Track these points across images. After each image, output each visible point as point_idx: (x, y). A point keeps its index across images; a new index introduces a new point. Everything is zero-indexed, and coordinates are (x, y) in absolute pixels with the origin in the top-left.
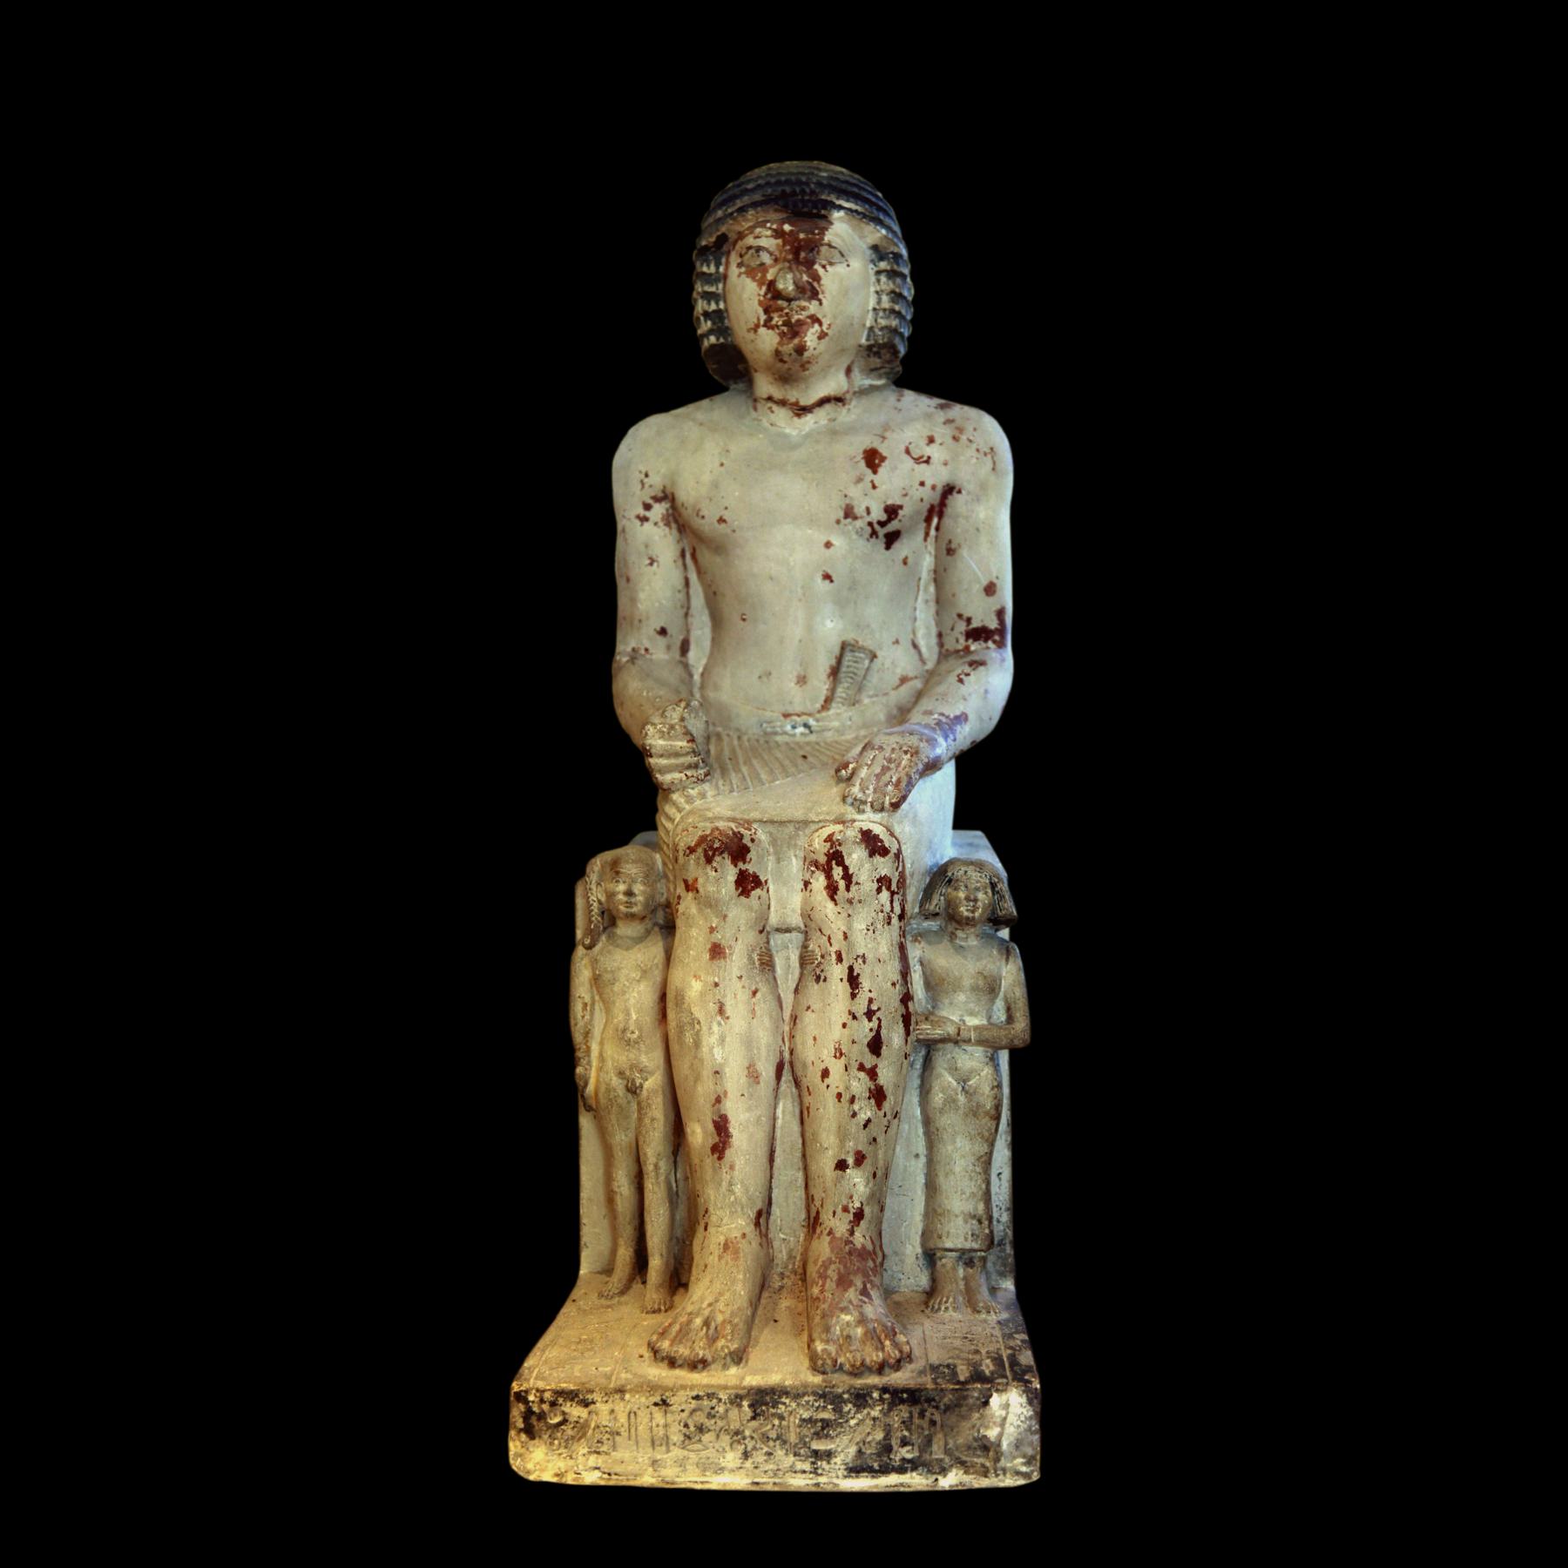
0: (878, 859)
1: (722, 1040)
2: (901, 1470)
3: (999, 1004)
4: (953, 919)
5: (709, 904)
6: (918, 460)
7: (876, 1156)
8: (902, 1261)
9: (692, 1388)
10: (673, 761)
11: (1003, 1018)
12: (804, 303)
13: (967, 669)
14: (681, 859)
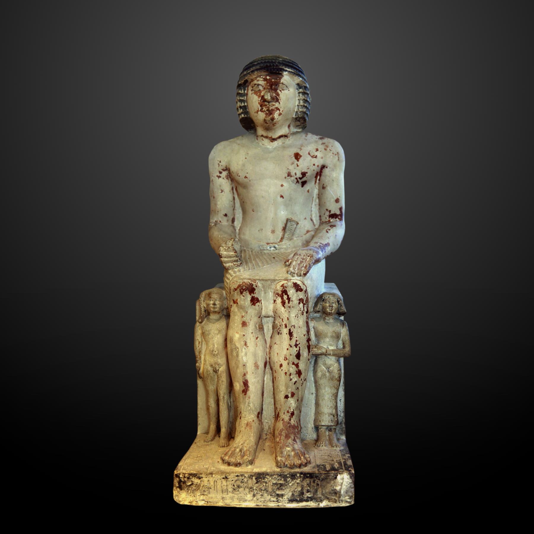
0: (299, 293)
1: (246, 354)
2: (307, 501)
3: (340, 342)
4: (325, 313)
5: (242, 308)
6: (313, 157)
7: (298, 394)
8: (307, 430)
9: (236, 473)
10: (229, 259)
11: (342, 347)
12: (274, 103)
13: (329, 228)
14: (232, 293)
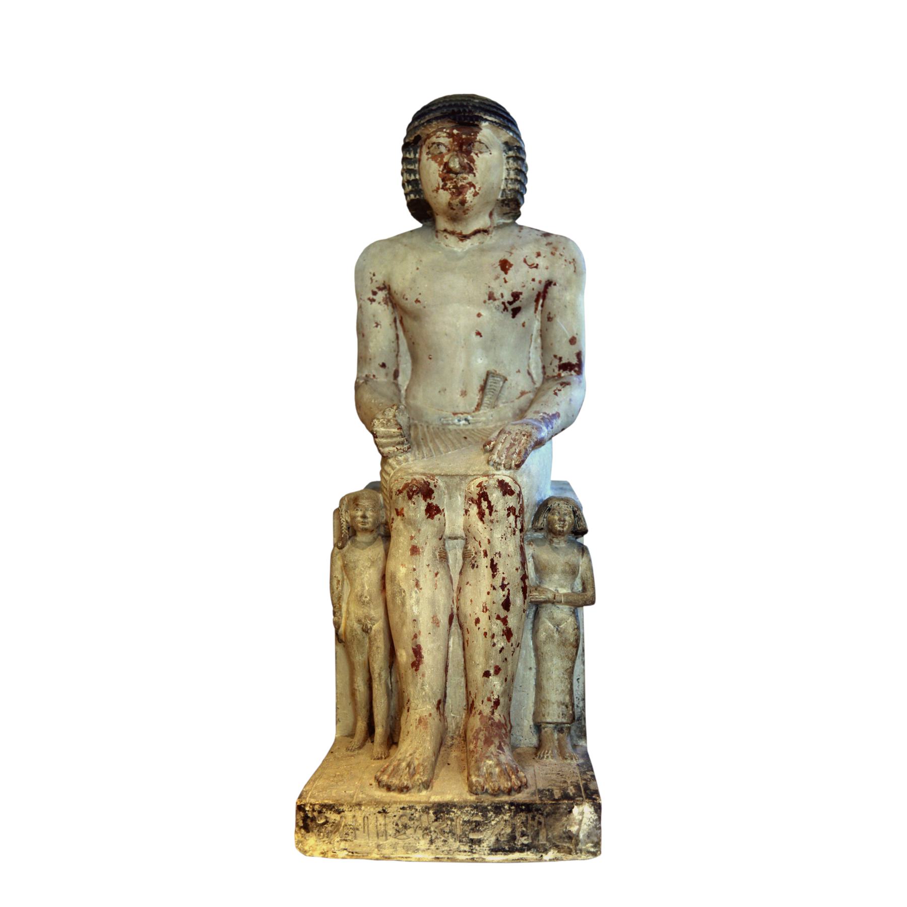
0: (508, 497)
1: (418, 602)
3: (578, 581)
5: (410, 523)
6: (531, 266)
7: (506, 668)
8: (522, 730)
9: (400, 803)
10: (389, 440)
11: (580, 589)
12: (465, 175)
13: (559, 387)
14: (394, 497)
